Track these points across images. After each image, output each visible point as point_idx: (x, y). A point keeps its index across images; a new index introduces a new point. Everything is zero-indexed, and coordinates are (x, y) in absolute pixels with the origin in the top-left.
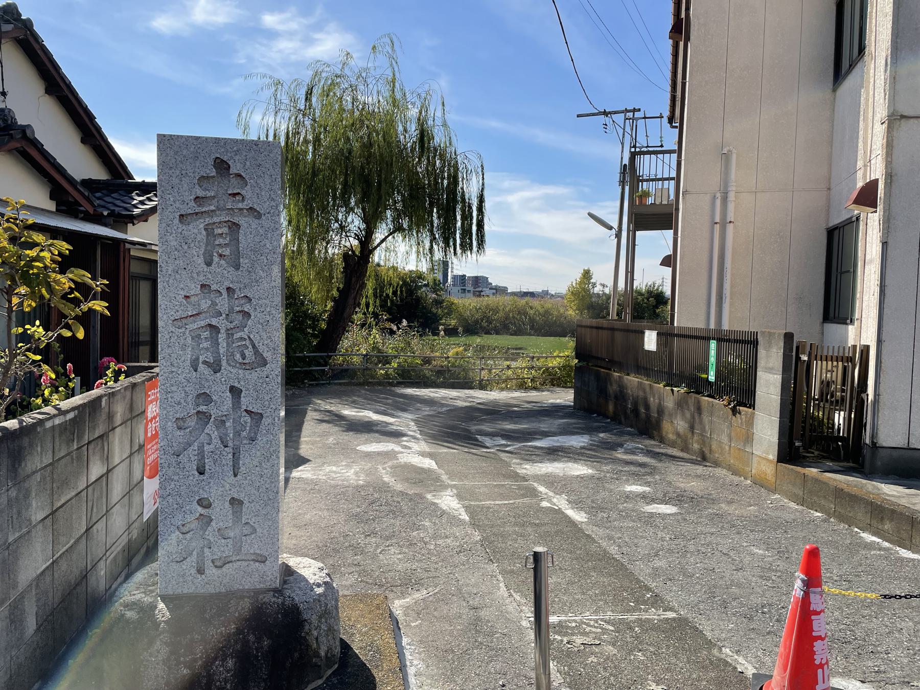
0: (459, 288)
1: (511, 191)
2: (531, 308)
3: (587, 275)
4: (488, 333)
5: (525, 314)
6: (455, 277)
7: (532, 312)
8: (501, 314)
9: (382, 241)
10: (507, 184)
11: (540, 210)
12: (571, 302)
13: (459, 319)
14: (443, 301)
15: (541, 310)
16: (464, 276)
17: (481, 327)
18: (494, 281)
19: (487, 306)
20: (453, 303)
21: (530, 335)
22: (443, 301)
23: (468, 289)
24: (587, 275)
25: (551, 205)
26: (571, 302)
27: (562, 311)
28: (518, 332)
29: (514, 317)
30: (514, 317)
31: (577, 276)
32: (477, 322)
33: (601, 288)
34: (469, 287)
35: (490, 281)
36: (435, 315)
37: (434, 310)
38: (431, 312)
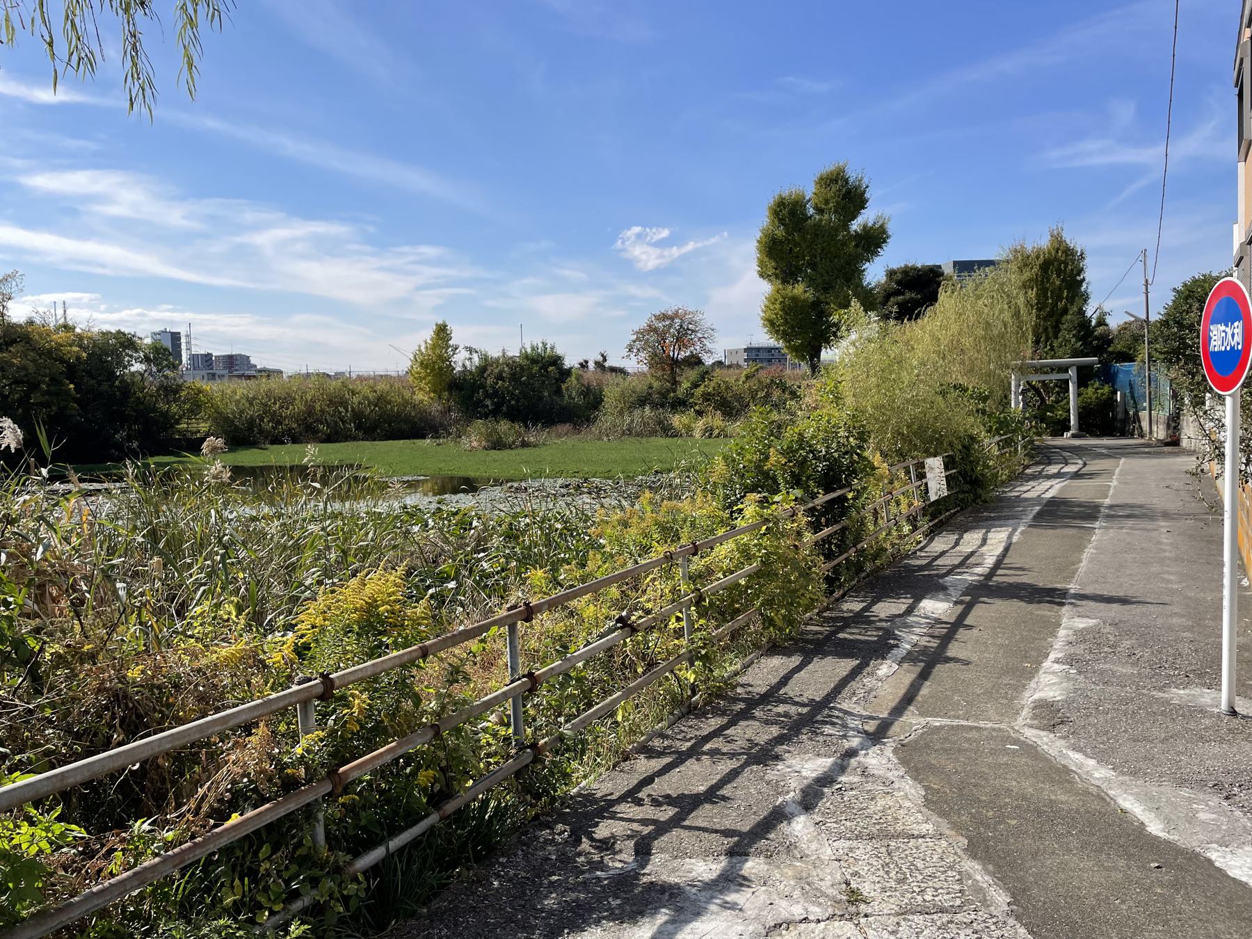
0: (204, 372)
1: (257, 227)
2: (354, 393)
3: (442, 332)
4: (277, 441)
5: (344, 403)
6: (193, 358)
7: (355, 400)
8: (299, 407)
9: (699, 829)
10: (249, 216)
11: (304, 257)
12: (421, 379)
13: (215, 419)
14: (179, 388)
15: (371, 396)
16: (209, 355)
17: (261, 431)
18: (259, 361)
19: (269, 394)
20: (200, 391)
21: (355, 439)
22: (179, 388)
23: (218, 372)
24: (442, 332)
25: (325, 249)
26: (421, 379)
27: (407, 394)
28: (333, 437)
29: (322, 411)
30: (322, 411)
31: (428, 334)
32: (251, 423)
33: (467, 355)
34: (219, 369)
35: (253, 361)
36: (165, 415)
37: (162, 406)
38: (154, 409)
